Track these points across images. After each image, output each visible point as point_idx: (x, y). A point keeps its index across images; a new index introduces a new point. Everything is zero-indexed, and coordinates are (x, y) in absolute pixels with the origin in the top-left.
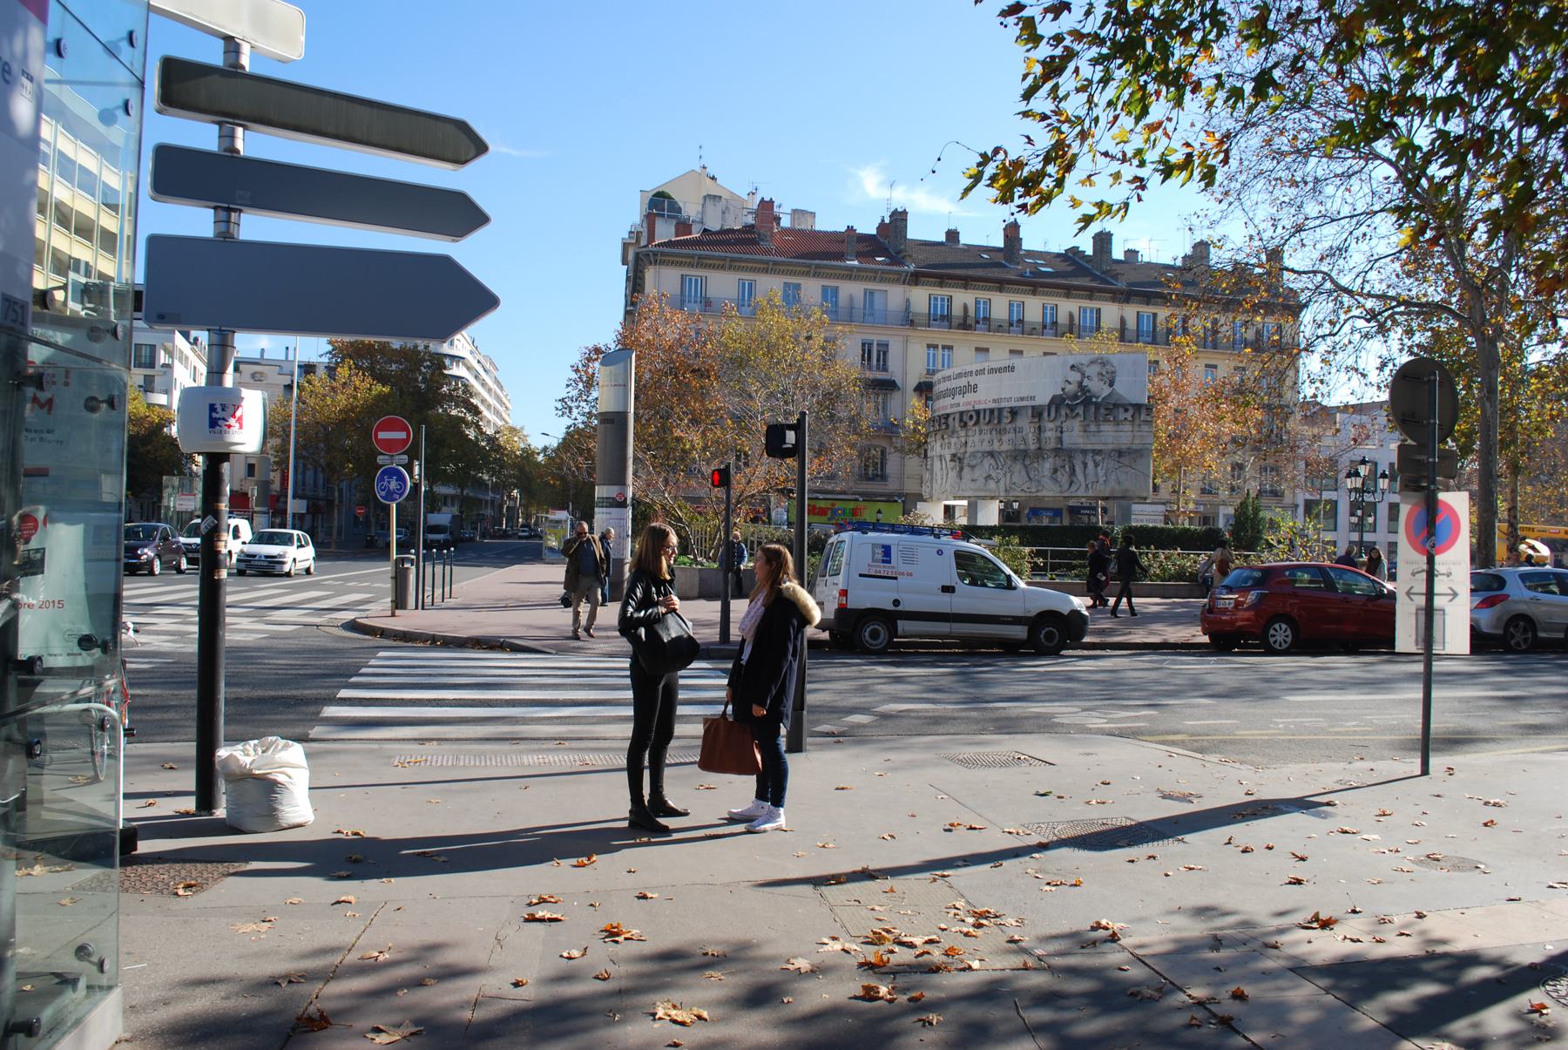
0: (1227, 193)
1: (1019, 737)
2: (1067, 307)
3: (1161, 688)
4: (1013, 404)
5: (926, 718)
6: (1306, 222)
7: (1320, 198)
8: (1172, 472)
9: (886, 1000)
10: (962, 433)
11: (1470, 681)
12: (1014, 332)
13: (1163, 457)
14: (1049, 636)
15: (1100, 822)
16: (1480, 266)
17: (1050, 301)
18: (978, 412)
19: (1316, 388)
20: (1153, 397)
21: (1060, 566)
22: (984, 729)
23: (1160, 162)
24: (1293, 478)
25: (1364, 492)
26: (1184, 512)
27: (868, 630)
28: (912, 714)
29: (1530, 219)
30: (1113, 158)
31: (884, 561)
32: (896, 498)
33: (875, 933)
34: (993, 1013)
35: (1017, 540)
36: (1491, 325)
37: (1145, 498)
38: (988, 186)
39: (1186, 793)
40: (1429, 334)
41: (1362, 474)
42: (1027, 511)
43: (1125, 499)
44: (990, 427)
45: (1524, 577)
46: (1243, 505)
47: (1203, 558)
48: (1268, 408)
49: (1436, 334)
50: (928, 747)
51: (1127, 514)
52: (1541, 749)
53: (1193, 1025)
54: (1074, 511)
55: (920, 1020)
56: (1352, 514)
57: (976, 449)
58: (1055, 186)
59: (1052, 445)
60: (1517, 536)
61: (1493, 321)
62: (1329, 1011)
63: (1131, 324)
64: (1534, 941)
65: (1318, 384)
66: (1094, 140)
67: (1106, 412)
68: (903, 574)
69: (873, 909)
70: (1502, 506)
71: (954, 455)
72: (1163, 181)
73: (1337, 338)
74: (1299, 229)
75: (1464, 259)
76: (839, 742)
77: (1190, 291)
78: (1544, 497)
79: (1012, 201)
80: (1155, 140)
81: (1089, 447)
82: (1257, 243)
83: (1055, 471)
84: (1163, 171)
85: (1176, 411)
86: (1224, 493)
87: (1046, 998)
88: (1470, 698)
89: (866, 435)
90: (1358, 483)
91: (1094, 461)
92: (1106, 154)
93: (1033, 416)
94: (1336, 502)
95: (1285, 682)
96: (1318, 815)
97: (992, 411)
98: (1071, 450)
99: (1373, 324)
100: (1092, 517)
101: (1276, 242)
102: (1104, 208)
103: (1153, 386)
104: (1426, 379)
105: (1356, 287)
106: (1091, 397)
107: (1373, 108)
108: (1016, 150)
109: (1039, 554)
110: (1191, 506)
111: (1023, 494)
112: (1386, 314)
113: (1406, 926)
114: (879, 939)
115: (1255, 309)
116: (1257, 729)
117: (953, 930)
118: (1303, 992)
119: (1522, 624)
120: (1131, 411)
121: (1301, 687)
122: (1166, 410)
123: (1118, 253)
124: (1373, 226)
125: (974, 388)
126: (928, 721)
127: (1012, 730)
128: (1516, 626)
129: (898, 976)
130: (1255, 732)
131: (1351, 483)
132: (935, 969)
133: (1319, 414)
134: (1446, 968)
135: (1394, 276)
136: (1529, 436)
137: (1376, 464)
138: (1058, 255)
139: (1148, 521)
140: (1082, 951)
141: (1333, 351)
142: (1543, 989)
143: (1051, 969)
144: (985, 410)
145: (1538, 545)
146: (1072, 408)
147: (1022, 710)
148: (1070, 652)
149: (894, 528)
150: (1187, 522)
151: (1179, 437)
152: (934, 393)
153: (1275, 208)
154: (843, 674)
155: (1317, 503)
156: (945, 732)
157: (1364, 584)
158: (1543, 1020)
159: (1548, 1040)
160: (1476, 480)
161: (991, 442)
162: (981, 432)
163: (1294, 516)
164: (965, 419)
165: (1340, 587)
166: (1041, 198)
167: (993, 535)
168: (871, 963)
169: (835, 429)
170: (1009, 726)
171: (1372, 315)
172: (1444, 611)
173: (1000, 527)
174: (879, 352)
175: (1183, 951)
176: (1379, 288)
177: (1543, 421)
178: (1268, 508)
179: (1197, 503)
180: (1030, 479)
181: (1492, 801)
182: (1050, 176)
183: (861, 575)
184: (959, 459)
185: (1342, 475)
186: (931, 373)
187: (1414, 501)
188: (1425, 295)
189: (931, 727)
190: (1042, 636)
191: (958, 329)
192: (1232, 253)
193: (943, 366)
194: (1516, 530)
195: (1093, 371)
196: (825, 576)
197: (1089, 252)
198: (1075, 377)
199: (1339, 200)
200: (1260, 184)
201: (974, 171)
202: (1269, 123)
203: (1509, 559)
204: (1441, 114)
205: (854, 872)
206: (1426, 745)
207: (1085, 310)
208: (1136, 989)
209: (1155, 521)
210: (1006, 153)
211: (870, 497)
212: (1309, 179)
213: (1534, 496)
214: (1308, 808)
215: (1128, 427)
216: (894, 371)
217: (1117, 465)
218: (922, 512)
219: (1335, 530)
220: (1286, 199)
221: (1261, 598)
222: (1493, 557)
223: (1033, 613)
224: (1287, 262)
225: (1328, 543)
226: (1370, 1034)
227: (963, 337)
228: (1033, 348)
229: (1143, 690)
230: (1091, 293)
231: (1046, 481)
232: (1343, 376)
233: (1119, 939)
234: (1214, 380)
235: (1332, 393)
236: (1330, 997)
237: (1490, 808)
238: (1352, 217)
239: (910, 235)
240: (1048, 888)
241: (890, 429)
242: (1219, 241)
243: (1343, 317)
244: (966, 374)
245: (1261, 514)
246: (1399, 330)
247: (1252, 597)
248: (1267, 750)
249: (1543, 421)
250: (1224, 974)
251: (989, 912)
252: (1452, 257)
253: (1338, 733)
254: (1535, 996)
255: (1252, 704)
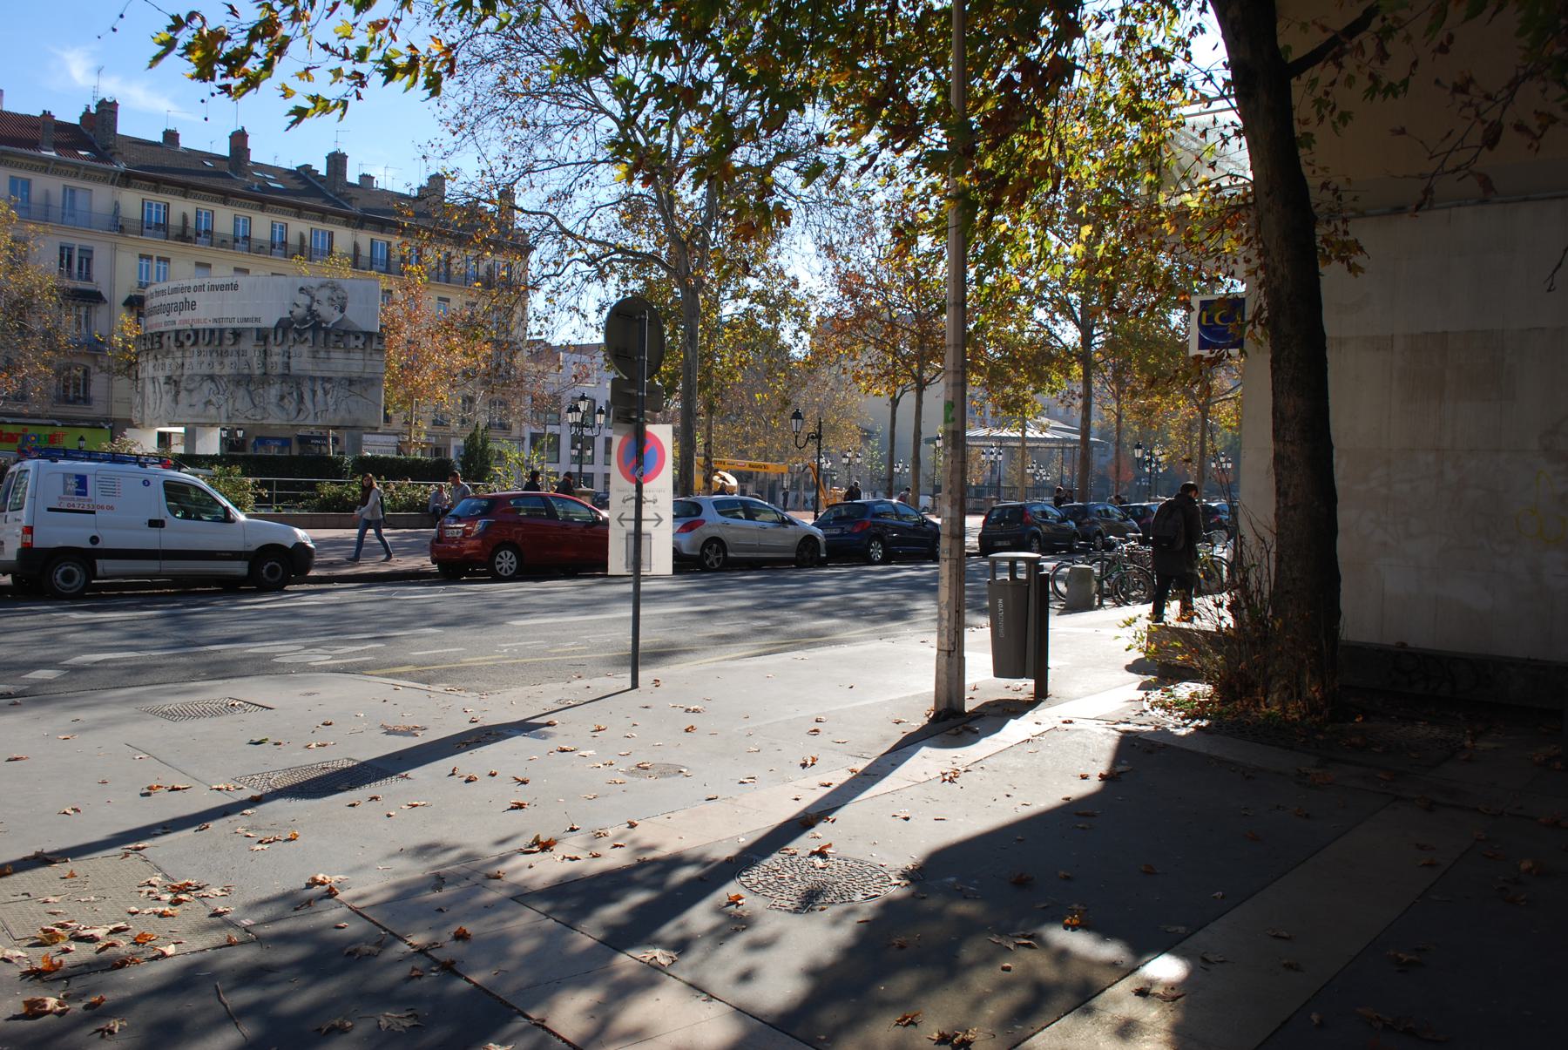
0: (461, 126)
1: (234, 681)
2: (298, 228)
3: (390, 619)
4: (236, 325)
5: (126, 668)
6: (535, 164)
7: (549, 142)
8: (404, 402)
9: (55, 1013)
10: (179, 354)
11: (673, 599)
12: (240, 248)
13: (396, 388)
14: (272, 571)
15: (320, 766)
16: (686, 223)
17: (280, 219)
18: (196, 332)
19: (541, 326)
20: (386, 327)
21: (287, 497)
22: (195, 676)
23: (381, 61)
24: (520, 412)
25: (584, 426)
26: (416, 443)
27: (60, 571)
28: (109, 665)
29: (730, 168)
30: (333, 52)
31: (78, 493)
32: (102, 424)
33: (45, 931)
34: (188, 1005)
35: (239, 471)
36: (694, 277)
37: (377, 428)
38: (181, 56)
39: (411, 726)
40: (642, 282)
41: (581, 410)
42: (253, 440)
43: (356, 429)
44: (209, 349)
45: (717, 504)
46: (473, 436)
47: (433, 488)
48: (498, 344)
49: (648, 282)
50: (128, 700)
51: (357, 444)
52: (729, 656)
53: (413, 978)
54: (304, 440)
55: (98, 1031)
56: (573, 447)
57: (195, 371)
58: (264, 69)
59: (279, 370)
60: (712, 468)
61: (696, 273)
62: (550, 936)
63: (365, 251)
64: (729, 835)
65: (543, 322)
66: (309, 24)
67: (337, 339)
68: (102, 507)
69: (46, 902)
70: (700, 441)
71: (169, 378)
72: (385, 83)
73: (561, 279)
74: (529, 170)
75: (672, 215)
76: (16, 704)
77: (423, 222)
78: (733, 435)
79: (213, 79)
80: (380, 41)
81: (318, 374)
82: (489, 179)
83: (282, 398)
84: (385, 72)
85: (408, 342)
86: (455, 425)
87: (253, 975)
88: (673, 613)
89: (65, 351)
90: (578, 417)
91: (324, 389)
92: (326, 47)
93: (258, 339)
94: (559, 435)
95: (510, 607)
96: (538, 736)
97: (212, 331)
98: (299, 377)
99: (592, 268)
100: (323, 447)
101: (507, 180)
102: (321, 104)
103: (386, 315)
104: (637, 317)
105: (579, 231)
106: (320, 323)
107: (596, 41)
108: (216, 19)
109: (263, 485)
110: (423, 437)
111: (247, 422)
112: (604, 260)
113: (619, 837)
114: (51, 938)
115: (486, 243)
116: (481, 655)
117: (146, 912)
118: (525, 920)
119: (715, 545)
120: (362, 339)
121: (525, 611)
122: (399, 340)
123: (352, 177)
124: (596, 174)
125: (193, 306)
126: (129, 671)
127: (228, 674)
128: (710, 548)
129: (72, 980)
130: (481, 658)
131: (572, 418)
132: (121, 964)
133: (545, 352)
134: (655, 873)
135: (612, 226)
136: (723, 380)
137: (594, 401)
138: (290, 172)
139: (381, 451)
140: (294, 914)
141: (557, 290)
142: (738, 880)
143: (260, 940)
144: (204, 330)
145: (728, 476)
146: (300, 333)
147: (237, 652)
148: (296, 587)
149: (91, 456)
150: (419, 453)
151: (411, 368)
152: (146, 308)
153: (507, 147)
154: (27, 624)
155: (541, 436)
156: (148, 681)
157: (585, 513)
158: (739, 910)
159: (743, 929)
160: (679, 418)
161: (211, 365)
162: (200, 353)
163: (521, 449)
164: (181, 338)
165: (560, 514)
166: (247, 80)
167: (213, 464)
168: (38, 970)
169: (26, 343)
170: (223, 670)
171: (592, 260)
172: (650, 535)
173: (222, 456)
174: (81, 259)
175: (404, 898)
176: (600, 235)
177: (734, 367)
178: (497, 440)
179: (428, 434)
180: (255, 406)
181: (692, 708)
182: (257, 56)
183: (50, 510)
184: (175, 381)
185: (564, 411)
186: (143, 286)
187: (625, 432)
188: (639, 246)
189: (132, 677)
190: (264, 571)
191: (176, 240)
192: (465, 186)
193: (158, 280)
194: (711, 462)
195: (323, 295)
196: (4, 511)
197: (323, 172)
198: (304, 300)
199: (567, 147)
200: (493, 120)
201: (165, 36)
202: (503, 62)
203: (704, 488)
204: (657, 58)
205: (25, 859)
206: (636, 659)
207: (317, 232)
208: (353, 947)
209: (388, 452)
210: (203, 19)
211: (71, 423)
212: (540, 123)
213: (725, 434)
214: (529, 731)
215: (358, 355)
216: (99, 280)
217: (347, 394)
218: (128, 439)
219: (558, 462)
220: (517, 139)
221: (487, 527)
222: (692, 489)
223: (254, 548)
224: (519, 202)
225: (551, 473)
226: (588, 953)
227: (182, 250)
228: (261, 268)
229: (370, 623)
230: (323, 216)
231: (273, 409)
232: (565, 316)
233: (336, 894)
234: (446, 312)
235: (555, 331)
236: (550, 921)
237: (691, 715)
238: (577, 164)
239: (120, 131)
240: (259, 847)
241: (95, 347)
242: (453, 173)
243: (567, 259)
244: (183, 290)
245: (490, 446)
246: (616, 276)
247: (479, 526)
248: (491, 676)
249: (734, 367)
250: (447, 915)
251: (190, 885)
252: (662, 212)
253: (557, 654)
254: (732, 889)
255: (479, 630)
